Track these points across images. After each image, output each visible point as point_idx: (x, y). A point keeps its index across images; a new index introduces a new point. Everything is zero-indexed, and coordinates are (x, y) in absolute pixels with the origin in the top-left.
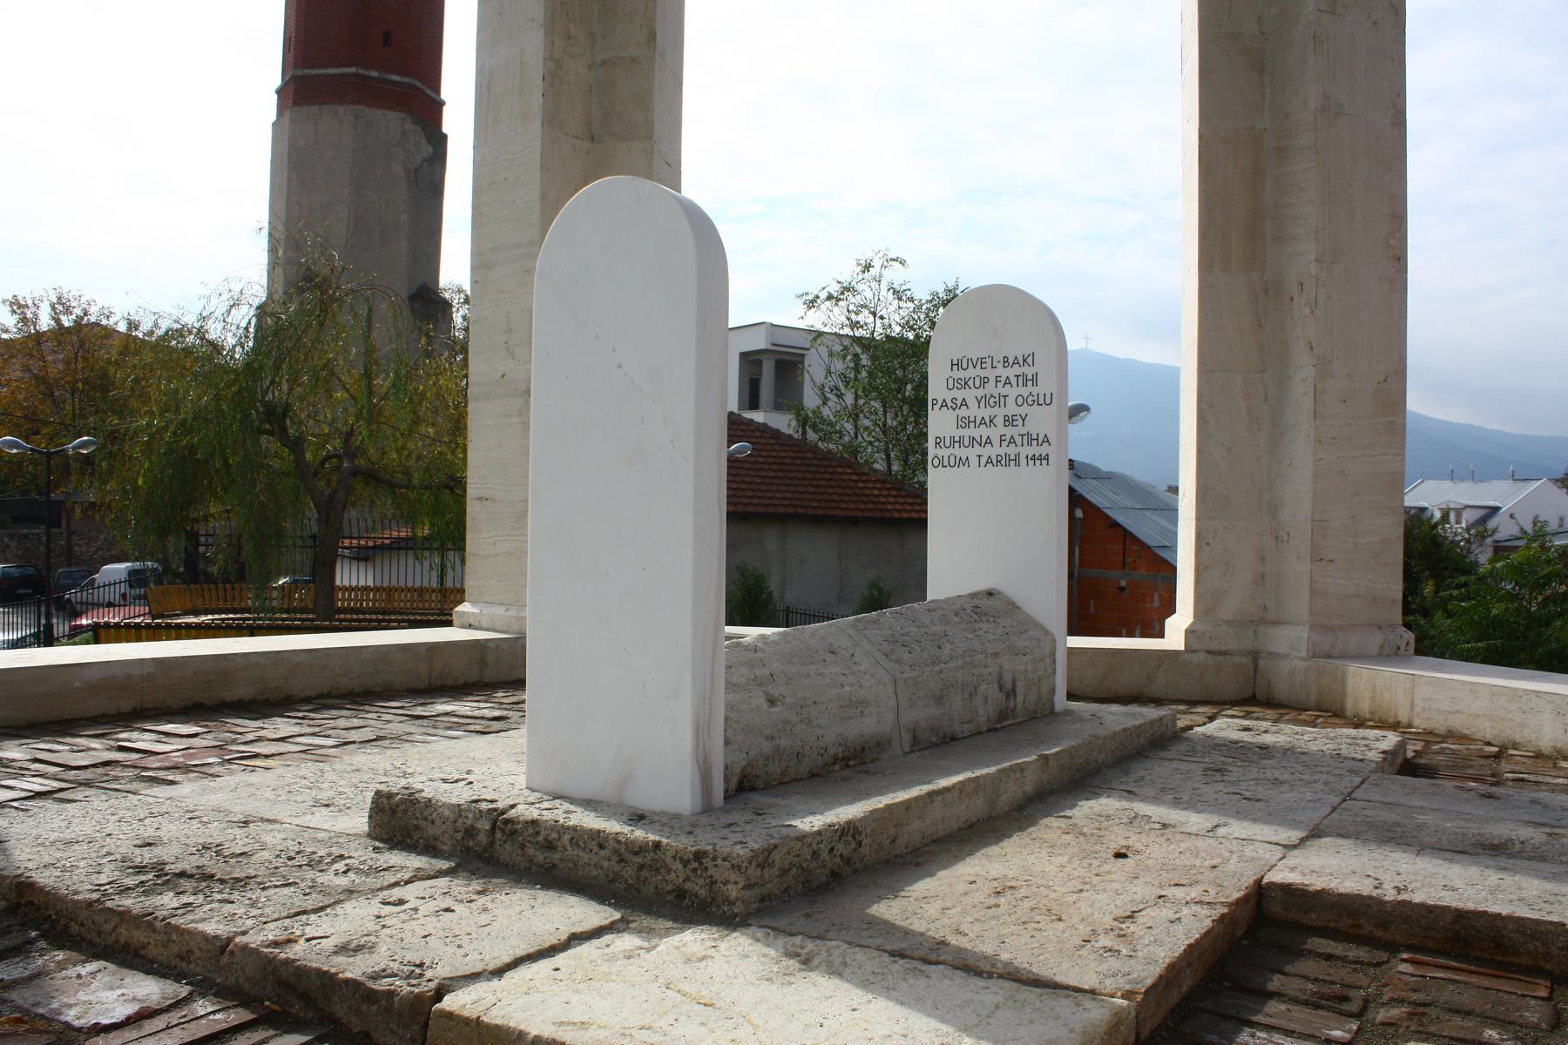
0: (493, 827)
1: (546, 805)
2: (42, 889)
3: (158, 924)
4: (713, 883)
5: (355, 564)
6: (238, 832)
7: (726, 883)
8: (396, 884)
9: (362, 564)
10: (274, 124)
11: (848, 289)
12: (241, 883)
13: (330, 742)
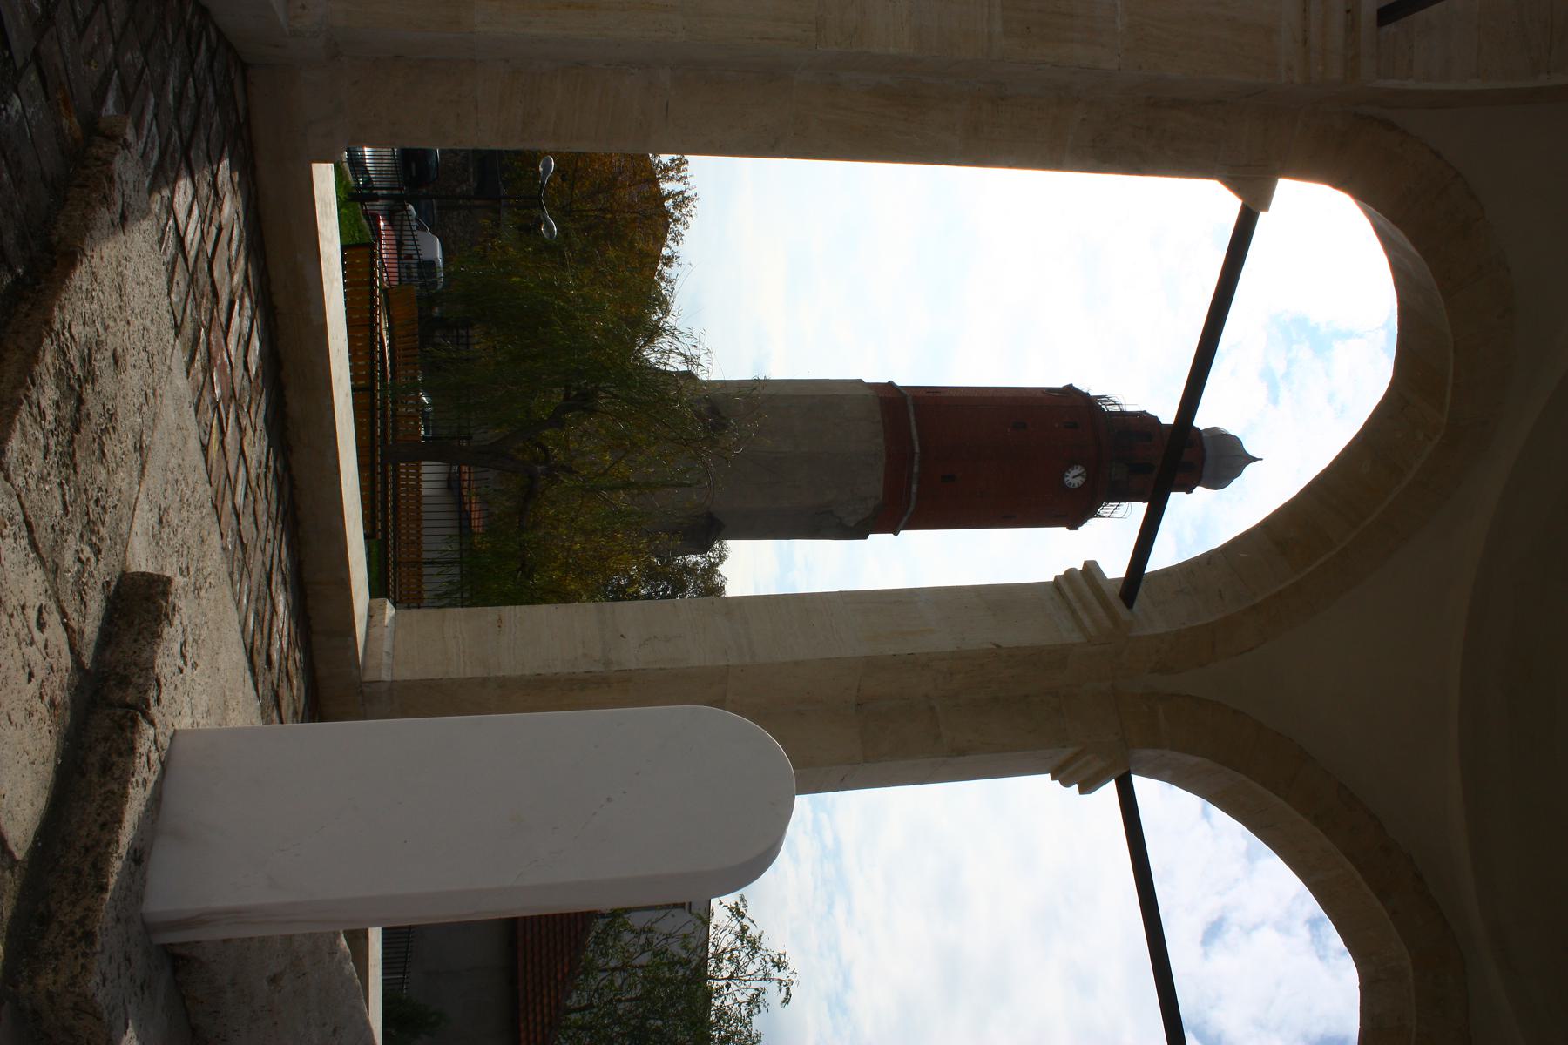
0: (128, 706)
1: (154, 756)
2: (67, 275)
3: (21, 392)
4: (56, 956)
5: (445, 477)
6: (130, 443)
7: (56, 971)
8: (64, 614)
9: (444, 484)
10: (861, 381)
11: (755, 946)
12: (68, 461)
13: (239, 498)
